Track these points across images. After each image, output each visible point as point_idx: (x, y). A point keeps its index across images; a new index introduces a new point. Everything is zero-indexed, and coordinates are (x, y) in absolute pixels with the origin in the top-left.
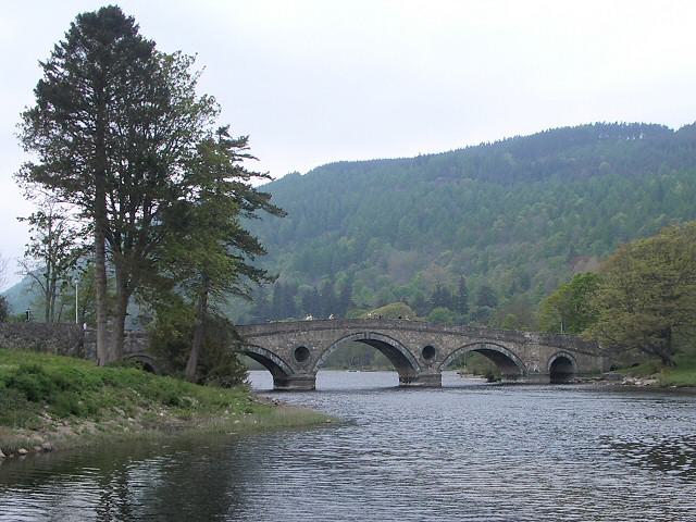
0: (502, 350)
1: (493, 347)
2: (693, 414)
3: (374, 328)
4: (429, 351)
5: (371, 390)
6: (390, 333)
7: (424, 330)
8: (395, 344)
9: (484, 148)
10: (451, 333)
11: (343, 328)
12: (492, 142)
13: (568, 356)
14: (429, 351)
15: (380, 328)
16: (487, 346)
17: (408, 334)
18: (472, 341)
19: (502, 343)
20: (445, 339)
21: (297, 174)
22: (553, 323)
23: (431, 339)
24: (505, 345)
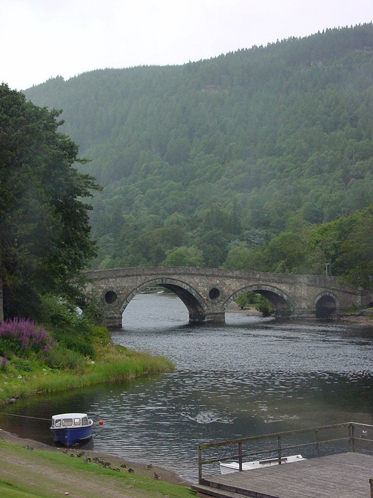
0: (276, 291)
1: (268, 288)
2: (372, 470)
3: (169, 274)
4: (214, 293)
5: (148, 332)
6: (183, 278)
7: (210, 275)
8: (186, 287)
9: (256, 51)
10: (232, 277)
11: (145, 275)
12: (265, 45)
13: (331, 295)
14: (214, 293)
15: (174, 274)
16: (263, 288)
17: (197, 280)
18: (250, 284)
19: (275, 285)
20: (228, 282)
21: (60, 79)
22: (181, 213)
23: (216, 282)
24: (278, 286)
